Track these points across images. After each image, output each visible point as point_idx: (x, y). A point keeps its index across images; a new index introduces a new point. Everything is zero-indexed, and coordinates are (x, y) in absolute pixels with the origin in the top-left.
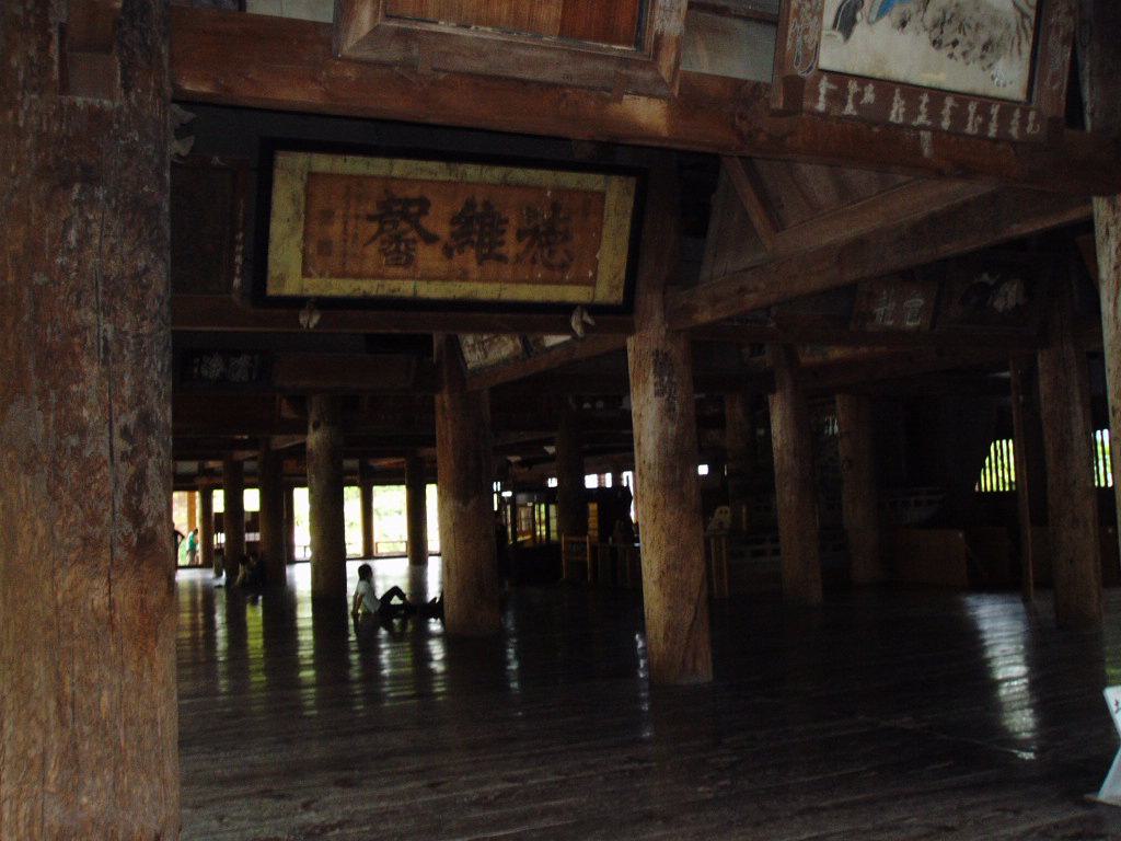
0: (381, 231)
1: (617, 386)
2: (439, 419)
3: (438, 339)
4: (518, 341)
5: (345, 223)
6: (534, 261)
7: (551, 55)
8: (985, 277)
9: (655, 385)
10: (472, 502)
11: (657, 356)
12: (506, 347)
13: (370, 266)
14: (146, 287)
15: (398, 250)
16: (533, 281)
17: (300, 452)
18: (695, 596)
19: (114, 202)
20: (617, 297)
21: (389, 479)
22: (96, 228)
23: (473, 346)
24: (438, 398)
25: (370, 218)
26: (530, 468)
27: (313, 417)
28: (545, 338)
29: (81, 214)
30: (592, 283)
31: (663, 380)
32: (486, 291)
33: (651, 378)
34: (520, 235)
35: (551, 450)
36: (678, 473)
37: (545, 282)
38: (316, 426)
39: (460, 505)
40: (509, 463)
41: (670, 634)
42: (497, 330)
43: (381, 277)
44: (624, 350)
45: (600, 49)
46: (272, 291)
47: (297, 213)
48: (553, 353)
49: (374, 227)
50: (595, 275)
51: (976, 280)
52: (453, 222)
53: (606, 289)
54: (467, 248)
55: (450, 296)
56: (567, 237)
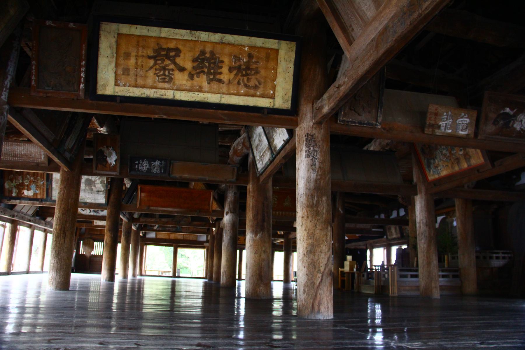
0: (155, 64)
5: (137, 59)
6: (239, 83)
8: (508, 110)
9: (306, 152)
10: (259, 235)
11: (308, 136)
13: (149, 82)
15: (164, 74)
16: (238, 94)
18: (322, 269)
20: (287, 105)
25: (150, 57)
27: (226, 209)
30: (273, 97)
31: (310, 149)
33: (304, 149)
34: (231, 70)
36: (316, 199)
37: (246, 95)
38: (227, 213)
41: (306, 290)
46: (100, 92)
49: (152, 62)
50: (274, 93)
51: (502, 111)
54: (201, 75)
55: (193, 100)
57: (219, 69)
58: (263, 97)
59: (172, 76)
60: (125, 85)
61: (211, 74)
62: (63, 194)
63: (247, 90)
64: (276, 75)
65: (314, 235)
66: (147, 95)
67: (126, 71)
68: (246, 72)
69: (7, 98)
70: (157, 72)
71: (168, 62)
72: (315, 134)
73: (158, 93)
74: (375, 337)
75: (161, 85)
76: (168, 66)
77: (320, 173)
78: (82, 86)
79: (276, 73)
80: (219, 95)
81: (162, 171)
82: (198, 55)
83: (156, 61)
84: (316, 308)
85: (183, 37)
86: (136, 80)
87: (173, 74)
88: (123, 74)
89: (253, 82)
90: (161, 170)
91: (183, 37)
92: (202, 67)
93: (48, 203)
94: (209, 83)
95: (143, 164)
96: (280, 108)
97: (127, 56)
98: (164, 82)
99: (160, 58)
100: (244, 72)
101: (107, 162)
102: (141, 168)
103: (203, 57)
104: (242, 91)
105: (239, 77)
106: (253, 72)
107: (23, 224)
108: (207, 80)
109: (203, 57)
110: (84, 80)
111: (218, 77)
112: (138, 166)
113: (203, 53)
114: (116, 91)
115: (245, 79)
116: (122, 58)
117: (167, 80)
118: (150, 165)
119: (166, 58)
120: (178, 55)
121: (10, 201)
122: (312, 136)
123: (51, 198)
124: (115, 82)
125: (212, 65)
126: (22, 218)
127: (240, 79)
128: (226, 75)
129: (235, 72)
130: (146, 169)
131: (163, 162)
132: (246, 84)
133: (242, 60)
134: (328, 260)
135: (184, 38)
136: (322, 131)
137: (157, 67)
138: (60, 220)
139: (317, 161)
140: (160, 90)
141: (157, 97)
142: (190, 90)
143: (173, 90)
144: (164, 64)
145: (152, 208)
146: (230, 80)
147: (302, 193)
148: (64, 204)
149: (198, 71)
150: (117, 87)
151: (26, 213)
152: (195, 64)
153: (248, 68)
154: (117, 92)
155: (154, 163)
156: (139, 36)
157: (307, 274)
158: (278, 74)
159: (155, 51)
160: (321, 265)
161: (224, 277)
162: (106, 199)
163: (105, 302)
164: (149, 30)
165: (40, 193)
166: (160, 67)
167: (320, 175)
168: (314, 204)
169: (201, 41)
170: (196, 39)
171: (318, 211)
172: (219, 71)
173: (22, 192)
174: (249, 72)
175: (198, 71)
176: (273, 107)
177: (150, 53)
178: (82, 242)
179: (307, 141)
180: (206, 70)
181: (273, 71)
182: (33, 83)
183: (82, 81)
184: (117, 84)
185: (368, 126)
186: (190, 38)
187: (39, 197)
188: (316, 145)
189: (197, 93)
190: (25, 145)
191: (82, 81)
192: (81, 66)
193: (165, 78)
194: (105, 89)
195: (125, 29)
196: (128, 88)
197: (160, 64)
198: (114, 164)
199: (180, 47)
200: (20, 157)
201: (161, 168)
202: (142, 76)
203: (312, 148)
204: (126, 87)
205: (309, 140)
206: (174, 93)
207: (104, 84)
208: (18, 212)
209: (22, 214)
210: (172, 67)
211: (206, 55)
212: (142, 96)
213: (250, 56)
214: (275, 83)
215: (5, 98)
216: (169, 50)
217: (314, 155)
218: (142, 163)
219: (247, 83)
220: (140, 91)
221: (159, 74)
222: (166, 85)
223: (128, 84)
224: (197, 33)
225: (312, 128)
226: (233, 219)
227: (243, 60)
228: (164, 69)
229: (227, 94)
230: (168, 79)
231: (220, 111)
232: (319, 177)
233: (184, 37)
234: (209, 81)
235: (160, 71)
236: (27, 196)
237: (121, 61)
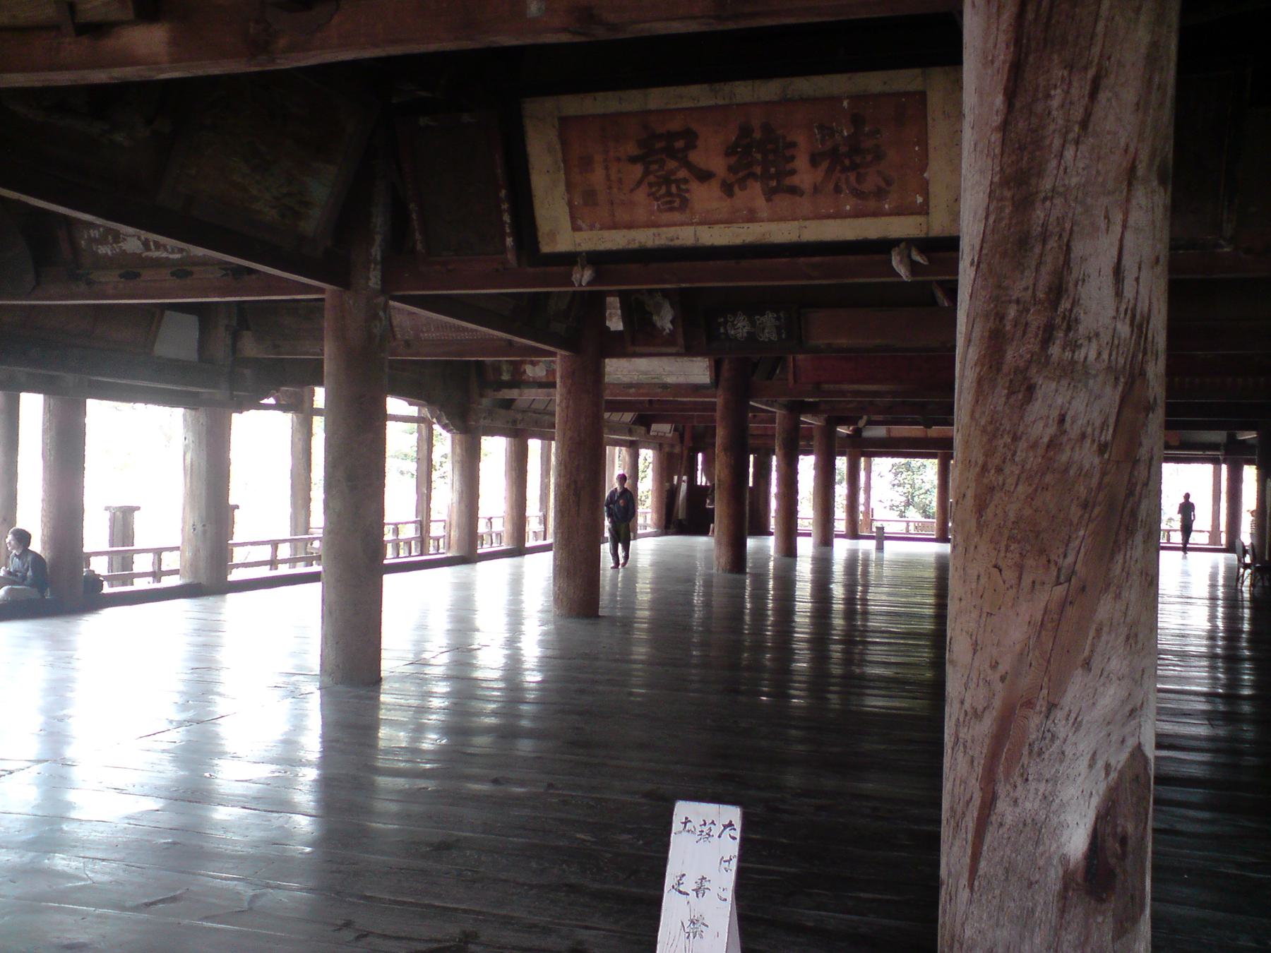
0: (647, 173)
5: (607, 168)
6: (837, 190)
15: (669, 194)
16: (839, 215)
25: (633, 160)
30: (924, 210)
34: (814, 160)
37: (858, 214)
46: (546, 248)
55: (738, 241)
58: (899, 214)
59: (687, 195)
60: (592, 228)
62: (567, 407)
63: (859, 202)
64: (927, 156)
66: (640, 242)
67: (590, 197)
69: (379, 283)
70: (654, 190)
71: (672, 164)
73: (663, 236)
74: (318, 772)
75: (666, 217)
79: (927, 150)
81: (784, 336)
82: (736, 139)
85: (696, 102)
89: (869, 185)
91: (696, 102)
94: (768, 200)
95: (735, 323)
97: (586, 163)
98: (671, 210)
100: (847, 162)
101: (654, 325)
102: (733, 332)
104: (848, 208)
106: (869, 158)
111: (789, 181)
112: (725, 328)
113: (745, 131)
114: (578, 240)
115: (852, 177)
117: (676, 205)
118: (753, 324)
120: (691, 145)
121: (501, 393)
125: (771, 157)
126: (536, 423)
128: (805, 176)
129: (825, 165)
130: (745, 335)
133: (837, 132)
137: (652, 178)
138: (566, 467)
140: (665, 229)
141: (662, 245)
142: (728, 222)
143: (692, 224)
144: (666, 168)
145: (826, 387)
146: (815, 184)
148: (570, 429)
149: (741, 174)
150: (577, 234)
151: (545, 409)
152: (732, 160)
154: (579, 245)
155: (762, 319)
156: (605, 116)
158: (931, 151)
162: (711, 371)
163: (561, 658)
164: (620, 99)
166: (657, 177)
168: (211, 761)
169: (738, 105)
170: (727, 101)
173: (522, 370)
174: (858, 160)
175: (741, 174)
176: (927, 234)
177: (631, 149)
178: (700, 456)
180: (758, 170)
181: (917, 149)
182: (419, 246)
183: (508, 230)
184: (576, 228)
185: (574, 922)
186: (711, 103)
189: (746, 225)
191: (508, 230)
195: (573, 105)
196: (600, 232)
198: (670, 330)
204: (594, 232)
206: (695, 231)
208: (524, 411)
209: (534, 415)
210: (683, 173)
211: (754, 135)
212: (632, 246)
213: (857, 121)
214: (925, 175)
215: (377, 284)
216: (671, 136)
218: (733, 322)
219: (857, 186)
220: (624, 236)
221: (658, 195)
222: (677, 216)
223: (597, 225)
224: (727, 88)
227: (842, 131)
229: (813, 218)
230: (677, 202)
231: (802, 259)
233: (698, 101)
234: (770, 194)
236: (533, 378)
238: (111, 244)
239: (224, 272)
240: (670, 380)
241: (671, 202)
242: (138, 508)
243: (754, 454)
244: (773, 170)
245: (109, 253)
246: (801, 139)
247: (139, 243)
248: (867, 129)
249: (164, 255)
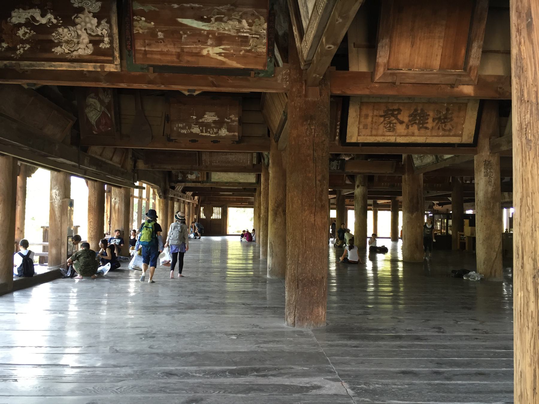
0: (384, 120)
1: (471, 173)
2: (403, 184)
3: (404, 156)
4: (434, 156)
5: (372, 118)
7: (436, 75)
9: (484, 173)
10: (415, 215)
11: (486, 162)
12: (429, 159)
13: (380, 132)
14: (324, 145)
15: (390, 127)
17: (351, 196)
18: (497, 250)
19: (317, 124)
20: (471, 141)
21: (384, 207)
22: (313, 130)
23: (417, 158)
24: (403, 177)
25: (381, 116)
26: (442, 207)
27: (357, 183)
28: (444, 155)
29: (310, 127)
30: (461, 136)
31: (487, 171)
32: (421, 140)
33: (483, 170)
34: (434, 120)
35: (450, 199)
36: (492, 204)
37: (443, 136)
38: (358, 186)
39: (410, 215)
40: (434, 204)
41: (486, 262)
42: (425, 153)
43: (384, 136)
44: (473, 161)
45: (452, 72)
46: (348, 141)
47: (357, 115)
48: (447, 161)
49: (382, 119)
50: (462, 133)
52: (409, 116)
53: (467, 136)
54: (414, 125)
55: (408, 142)
56: (452, 120)
57: (426, 120)
61: (421, 124)
65: (491, 228)
67: (365, 127)
68: (444, 121)
72: (491, 160)
76: (393, 121)
77: (495, 187)
78: (337, 138)
80: (425, 137)
81: (339, 168)
83: (385, 118)
84: (493, 274)
86: (371, 132)
87: (395, 126)
88: (363, 128)
89: (448, 127)
90: (337, 167)
92: (415, 120)
93: (208, 184)
94: (419, 130)
96: (466, 143)
97: (367, 116)
99: (388, 116)
100: (443, 121)
103: (416, 113)
104: (441, 134)
105: (439, 124)
107: (258, 216)
108: (418, 129)
109: (416, 113)
110: (338, 134)
111: (425, 125)
115: (443, 125)
116: (363, 118)
117: (391, 130)
119: (392, 116)
120: (399, 113)
122: (489, 161)
123: (211, 180)
124: (358, 134)
127: (440, 126)
129: (436, 121)
131: (339, 161)
132: (444, 129)
134: (500, 244)
135: (404, 102)
136: (496, 158)
137: (386, 122)
139: (492, 179)
140: (387, 137)
143: (395, 136)
147: (482, 200)
150: (359, 137)
153: (446, 118)
157: (486, 253)
159: (385, 112)
160: (496, 247)
161: (358, 240)
165: (201, 176)
166: (387, 122)
167: (495, 188)
171: (494, 212)
172: (426, 121)
173: (187, 176)
179: (485, 165)
183: (338, 135)
187: (200, 180)
188: (492, 168)
190: (236, 154)
191: (338, 135)
192: (336, 125)
193: (390, 129)
194: (351, 139)
197: (388, 120)
199: (401, 108)
200: (232, 163)
201: (337, 166)
202: (375, 129)
203: (489, 170)
205: (487, 165)
207: (351, 135)
212: (375, 142)
213: (448, 110)
216: (394, 110)
217: (490, 175)
219: (444, 128)
225: (489, 156)
226: (363, 191)
228: (390, 123)
229: (431, 136)
230: (392, 129)
232: (494, 190)
235: (388, 125)
236: (191, 179)
237: (362, 120)
238: (187, 130)
239: (232, 142)
240: (241, 181)
241: (390, 129)
242: (79, 226)
243: (463, 210)
244: (421, 122)
245: (186, 132)
246: (431, 114)
247: (199, 130)
248: (450, 112)
249: (209, 135)
